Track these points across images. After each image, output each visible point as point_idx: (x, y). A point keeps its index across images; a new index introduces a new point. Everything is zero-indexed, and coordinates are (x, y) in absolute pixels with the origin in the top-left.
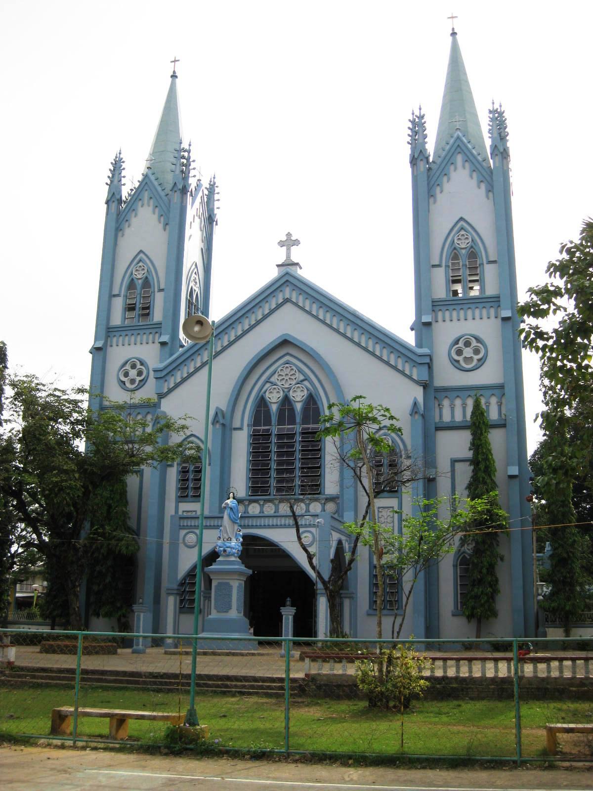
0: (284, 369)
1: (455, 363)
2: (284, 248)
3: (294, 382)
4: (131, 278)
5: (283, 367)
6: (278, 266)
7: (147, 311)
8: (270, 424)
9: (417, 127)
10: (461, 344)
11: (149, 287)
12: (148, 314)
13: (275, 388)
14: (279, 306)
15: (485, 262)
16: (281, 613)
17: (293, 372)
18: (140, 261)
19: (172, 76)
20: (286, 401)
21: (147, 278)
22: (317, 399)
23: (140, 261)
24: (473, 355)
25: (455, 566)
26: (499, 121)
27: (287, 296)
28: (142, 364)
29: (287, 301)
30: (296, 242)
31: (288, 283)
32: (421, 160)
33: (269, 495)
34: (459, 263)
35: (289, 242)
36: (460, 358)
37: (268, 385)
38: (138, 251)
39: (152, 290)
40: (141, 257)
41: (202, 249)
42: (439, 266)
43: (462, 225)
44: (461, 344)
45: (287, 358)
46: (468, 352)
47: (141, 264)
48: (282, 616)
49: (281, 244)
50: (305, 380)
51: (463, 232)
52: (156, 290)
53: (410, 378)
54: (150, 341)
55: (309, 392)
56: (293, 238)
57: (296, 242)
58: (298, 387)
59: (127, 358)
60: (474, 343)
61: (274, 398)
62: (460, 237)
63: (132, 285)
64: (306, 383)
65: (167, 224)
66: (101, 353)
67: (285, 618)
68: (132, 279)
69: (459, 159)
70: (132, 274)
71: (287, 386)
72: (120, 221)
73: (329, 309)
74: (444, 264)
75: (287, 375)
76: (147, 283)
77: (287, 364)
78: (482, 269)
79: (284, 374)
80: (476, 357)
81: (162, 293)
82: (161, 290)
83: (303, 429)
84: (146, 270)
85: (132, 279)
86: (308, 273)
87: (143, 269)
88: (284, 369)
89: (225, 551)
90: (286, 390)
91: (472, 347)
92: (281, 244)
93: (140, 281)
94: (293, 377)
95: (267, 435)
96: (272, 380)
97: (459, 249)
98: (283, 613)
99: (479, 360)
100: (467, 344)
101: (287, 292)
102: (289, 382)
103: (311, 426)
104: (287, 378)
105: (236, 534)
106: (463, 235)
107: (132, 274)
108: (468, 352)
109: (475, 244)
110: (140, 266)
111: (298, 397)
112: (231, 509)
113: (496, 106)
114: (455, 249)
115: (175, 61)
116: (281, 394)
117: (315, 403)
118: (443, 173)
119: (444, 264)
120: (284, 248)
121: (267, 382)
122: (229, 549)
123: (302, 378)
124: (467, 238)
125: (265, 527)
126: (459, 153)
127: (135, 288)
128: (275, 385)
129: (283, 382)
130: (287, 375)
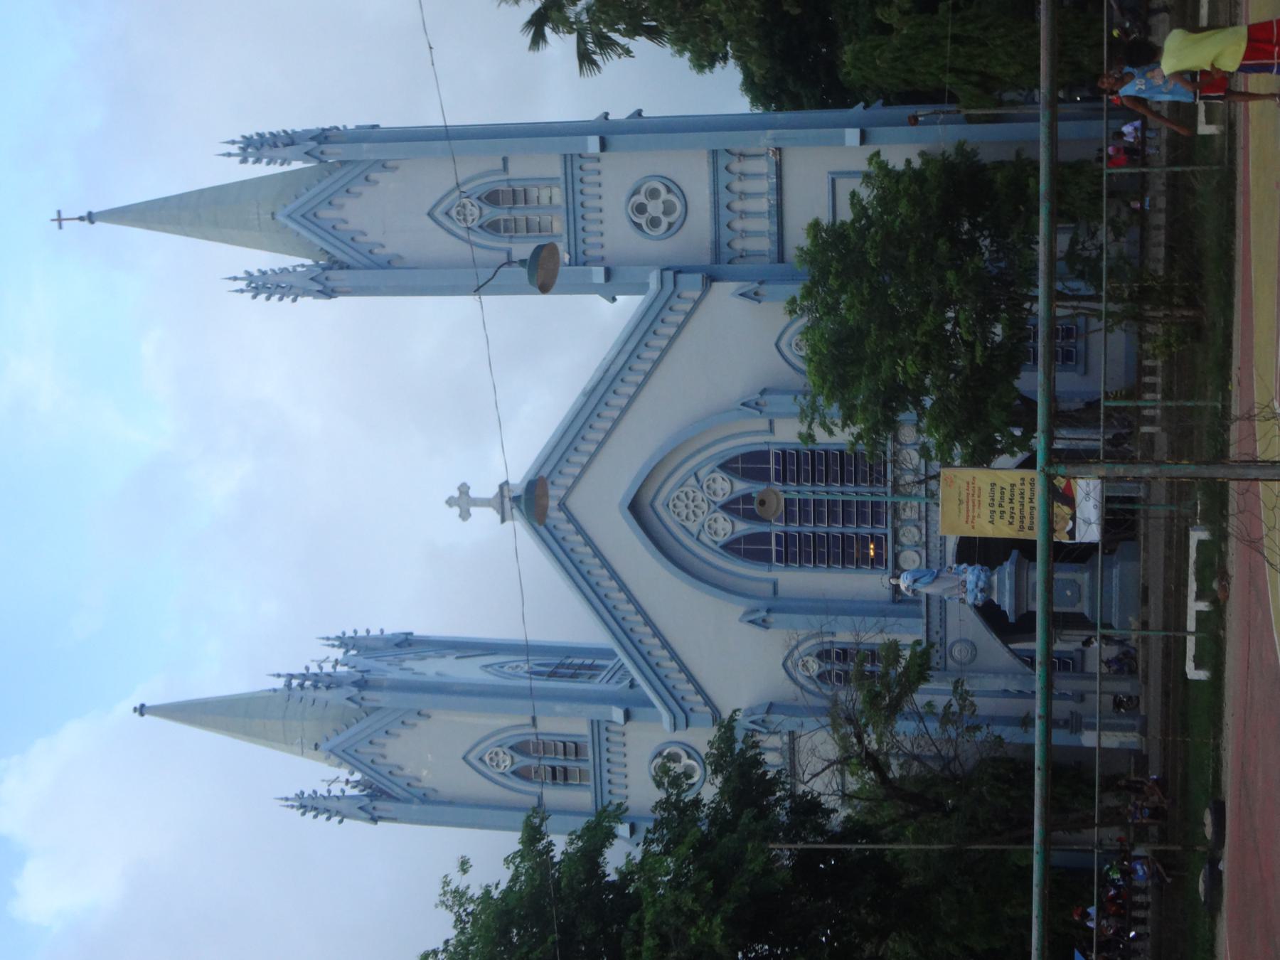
1: (672, 186)
2: (473, 510)
3: (699, 495)
4: (479, 230)
5: (674, 512)
8: (768, 535)
10: (642, 220)
13: (709, 527)
14: (571, 519)
17: (683, 496)
21: (511, 748)
23: (481, 759)
24: (660, 201)
26: (255, 147)
28: (638, 226)
29: (563, 506)
30: (464, 489)
33: (886, 535)
36: (665, 221)
38: (463, 763)
41: (457, 658)
43: (474, 761)
44: (642, 220)
46: (655, 208)
47: (487, 759)
49: (465, 515)
50: (696, 475)
51: (453, 213)
53: (697, 303)
55: (718, 470)
56: (456, 494)
57: (464, 489)
61: (726, 527)
64: (701, 474)
68: (514, 773)
69: (326, 214)
71: (705, 506)
73: (580, 436)
75: (687, 506)
76: (519, 748)
77: (668, 505)
80: (664, 195)
83: (777, 479)
84: (498, 749)
85: (481, 227)
86: (518, 476)
92: (465, 515)
93: (518, 758)
94: (691, 495)
99: (669, 190)
102: (699, 502)
103: (772, 466)
104: (692, 505)
107: (502, 774)
108: (655, 208)
110: (491, 759)
111: (726, 487)
113: (235, 149)
115: (59, 220)
116: (720, 515)
117: (735, 460)
119: (505, 245)
120: (473, 510)
123: (692, 481)
127: (528, 768)
128: (703, 526)
129: (699, 512)
130: (687, 506)
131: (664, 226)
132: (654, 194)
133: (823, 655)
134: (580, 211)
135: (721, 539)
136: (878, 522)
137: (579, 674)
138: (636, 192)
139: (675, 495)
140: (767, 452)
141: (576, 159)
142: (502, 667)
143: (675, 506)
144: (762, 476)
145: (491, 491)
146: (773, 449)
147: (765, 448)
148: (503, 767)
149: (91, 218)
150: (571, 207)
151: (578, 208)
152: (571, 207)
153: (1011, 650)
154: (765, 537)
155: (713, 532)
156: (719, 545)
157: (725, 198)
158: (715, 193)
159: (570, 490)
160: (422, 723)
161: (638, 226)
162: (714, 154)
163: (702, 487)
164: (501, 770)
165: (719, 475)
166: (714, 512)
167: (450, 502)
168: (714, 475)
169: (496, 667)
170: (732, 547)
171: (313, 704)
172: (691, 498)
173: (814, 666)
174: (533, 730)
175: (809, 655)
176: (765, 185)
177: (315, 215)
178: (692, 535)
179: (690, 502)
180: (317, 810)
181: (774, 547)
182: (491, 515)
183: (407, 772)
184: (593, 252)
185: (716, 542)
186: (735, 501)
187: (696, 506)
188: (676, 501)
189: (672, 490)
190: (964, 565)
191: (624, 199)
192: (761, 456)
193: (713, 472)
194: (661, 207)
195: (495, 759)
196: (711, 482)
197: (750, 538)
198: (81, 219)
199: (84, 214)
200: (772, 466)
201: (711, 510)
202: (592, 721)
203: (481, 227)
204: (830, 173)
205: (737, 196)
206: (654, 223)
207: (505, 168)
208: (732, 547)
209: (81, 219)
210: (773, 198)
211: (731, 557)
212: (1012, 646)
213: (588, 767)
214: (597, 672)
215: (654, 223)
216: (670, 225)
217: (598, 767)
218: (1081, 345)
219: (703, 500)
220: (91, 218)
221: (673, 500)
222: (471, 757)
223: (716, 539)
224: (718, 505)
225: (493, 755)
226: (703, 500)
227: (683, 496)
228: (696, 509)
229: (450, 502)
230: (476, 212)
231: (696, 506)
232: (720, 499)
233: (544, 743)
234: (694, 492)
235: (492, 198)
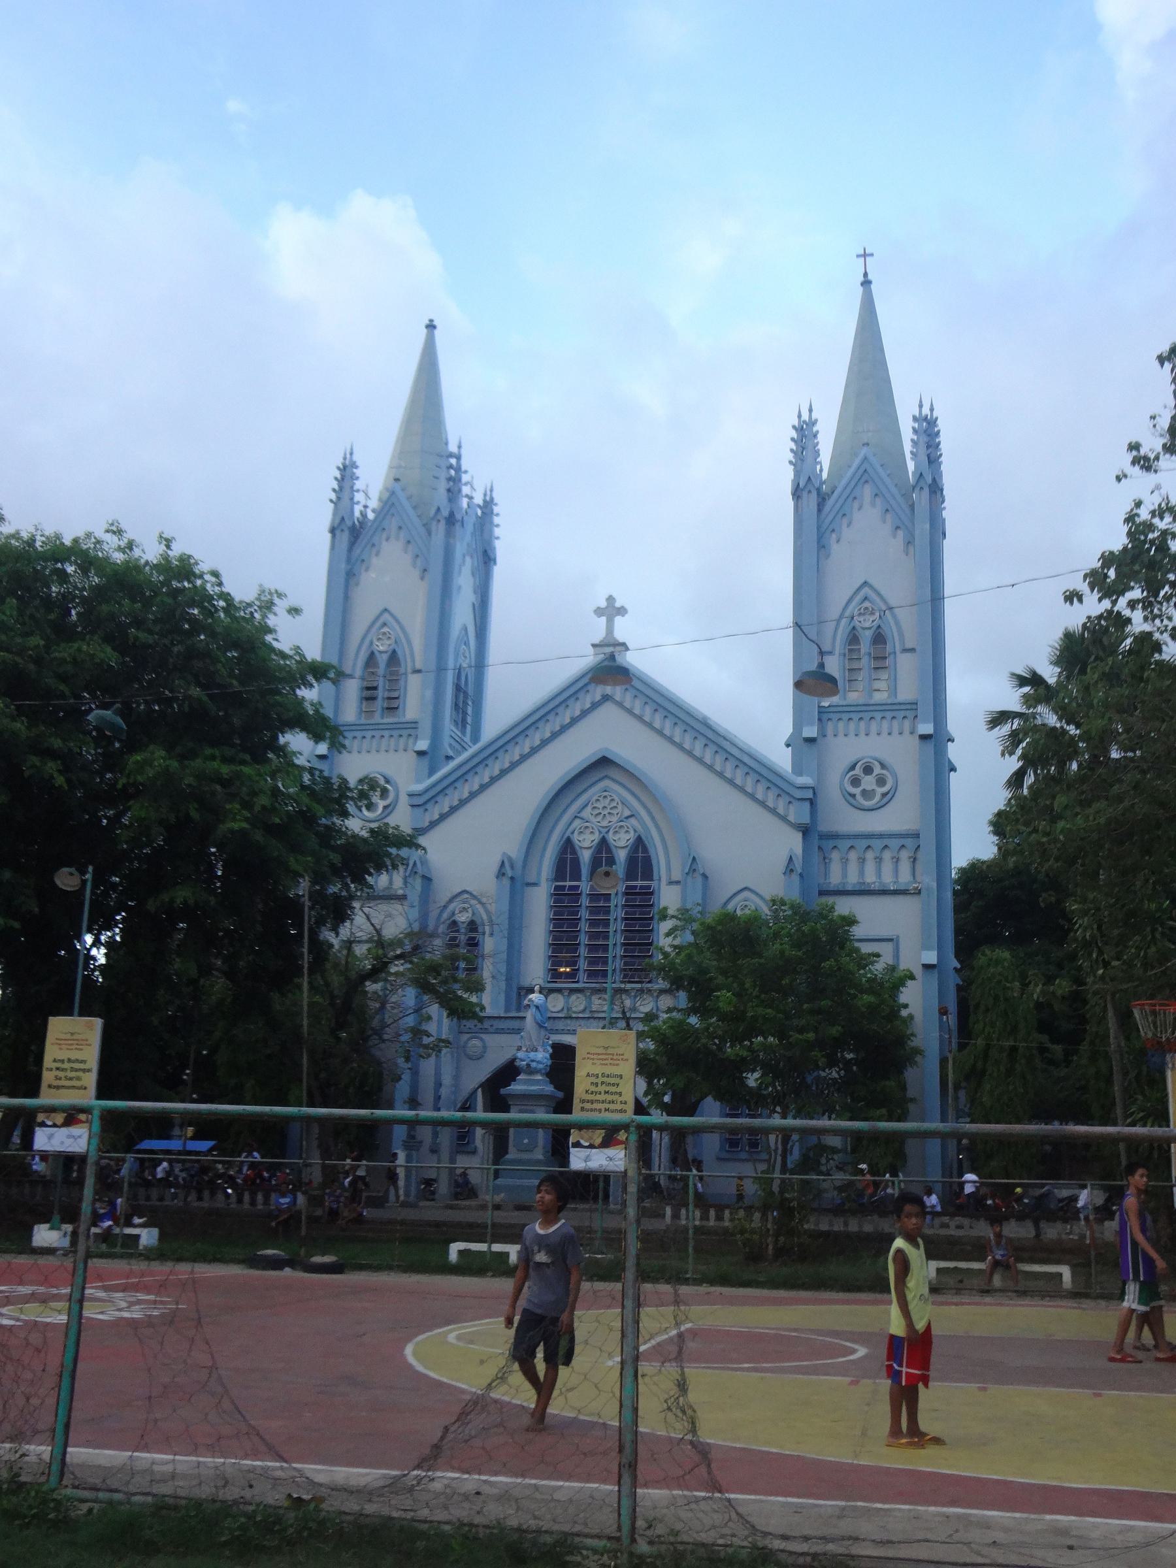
3: (615, 819)
6: (594, 646)
8: (579, 879)
9: (805, 434)
10: (858, 771)
14: (595, 706)
18: (866, 598)
19: (428, 327)
20: (603, 848)
23: (385, 624)
24: (874, 787)
26: (928, 429)
29: (606, 698)
30: (622, 611)
35: (612, 610)
36: (857, 791)
38: (381, 608)
41: (474, 604)
44: (858, 771)
46: (868, 782)
47: (385, 629)
49: (599, 612)
53: (784, 818)
54: (852, 733)
56: (618, 605)
57: (622, 611)
59: (853, 759)
61: (586, 843)
63: (371, 660)
64: (633, 821)
69: (867, 491)
71: (605, 823)
74: (837, 652)
76: (394, 659)
80: (880, 790)
85: (854, 628)
86: (633, 659)
88: (601, 799)
91: (874, 774)
92: (599, 612)
93: (385, 657)
94: (614, 812)
95: (575, 894)
96: (582, 815)
97: (859, 629)
99: (884, 795)
103: (639, 883)
108: (868, 782)
111: (621, 842)
112: (537, 1007)
113: (926, 411)
116: (596, 837)
117: (645, 850)
118: (863, 480)
119: (837, 652)
121: (576, 817)
123: (627, 813)
127: (376, 665)
129: (599, 818)
132: (881, 781)
133: (473, 926)
134: (867, 716)
135: (576, 838)
136: (589, 976)
138: (883, 766)
139: (615, 797)
142: (465, 644)
143: (605, 797)
144: (631, 874)
145: (620, 635)
146: (654, 884)
147: (655, 876)
149: (866, 283)
151: (902, 714)
153: (475, 1091)
154: (576, 876)
157: (877, 844)
158: (881, 836)
159: (620, 705)
161: (853, 767)
162: (916, 836)
165: (632, 836)
166: (600, 832)
167: (611, 599)
170: (568, 847)
173: (463, 918)
174: (409, 670)
175: (474, 914)
176: (888, 880)
177: (866, 482)
180: (341, 481)
181: (568, 884)
182: (599, 635)
184: (830, 727)
185: (573, 833)
188: (609, 798)
189: (619, 795)
190: (551, 1050)
191: (878, 755)
192: (648, 873)
193: (635, 831)
194: (869, 788)
197: (576, 862)
198: (866, 274)
199: (870, 277)
200: (639, 883)
201: (601, 829)
202: (416, 722)
203: (854, 628)
204: (898, 937)
206: (856, 782)
207: (905, 650)
209: (866, 274)
210: (877, 887)
212: (480, 1090)
213: (377, 718)
215: (856, 782)
216: (853, 796)
217: (377, 727)
220: (866, 283)
224: (606, 836)
229: (611, 599)
230: (867, 625)
232: (611, 837)
235: (879, 638)
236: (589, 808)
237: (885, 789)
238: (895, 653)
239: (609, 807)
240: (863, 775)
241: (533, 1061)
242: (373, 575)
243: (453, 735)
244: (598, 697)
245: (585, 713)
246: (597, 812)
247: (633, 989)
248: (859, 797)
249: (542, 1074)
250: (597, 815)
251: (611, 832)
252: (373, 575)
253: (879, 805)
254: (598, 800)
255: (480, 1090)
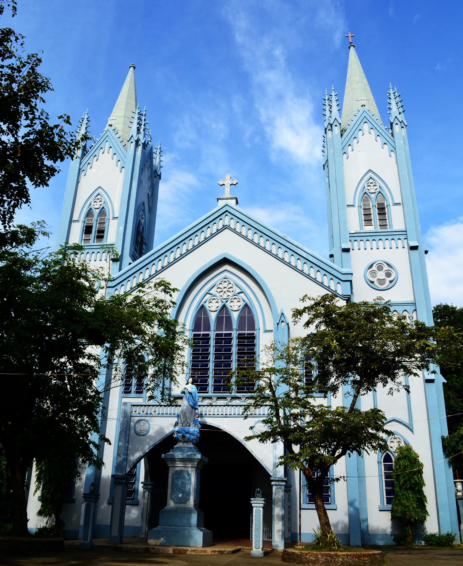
0: (222, 283)
3: (231, 294)
5: (222, 281)
7: (101, 235)
8: (209, 330)
10: (374, 268)
11: (105, 215)
12: (102, 237)
13: (214, 299)
14: (219, 231)
15: (391, 204)
16: (251, 504)
17: (230, 286)
22: (252, 310)
24: (385, 277)
25: (379, 463)
27: (227, 223)
29: (225, 227)
31: (227, 213)
32: (336, 126)
33: (207, 393)
34: (369, 205)
36: (375, 280)
37: (208, 296)
38: (98, 186)
39: (107, 217)
40: (99, 192)
41: (148, 194)
42: (353, 206)
45: (226, 274)
47: (99, 197)
48: (252, 508)
50: (242, 292)
52: (111, 218)
55: (245, 303)
58: (235, 298)
60: (386, 268)
62: (369, 184)
63: (89, 214)
64: (242, 295)
65: (123, 167)
66: (118, 263)
67: (256, 512)
68: (91, 209)
69: (366, 127)
70: (91, 204)
71: (225, 296)
72: (83, 164)
74: (357, 205)
75: (225, 288)
76: (102, 212)
77: (225, 278)
78: (389, 209)
79: (222, 287)
81: (116, 221)
82: (114, 218)
83: (239, 334)
84: (103, 202)
85: (91, 209)
87: (101, 201)
88: (222, 283)
89: (183, 436)
90: (224, 301)
91: (384, 270)
93: (98, 211)
94: (231, 290)
95: (206, 338)
96: (211, 292)
97: (369, 194)
98: (253, 505)
99: (391, 282)
100: (380, 268)
101: (226, 220)
103: (246, 332)
104: (225, 290)
105: (194, 420)
106: (371, 183)
107: (91, 204)
109: (381, 189)
110: (98, 199)
112: (190, 393)
114: (365, 193)
116: (220, 305)
117: (250, 312)
118: (358, 129)
119: (357, 205)
121: (207, 293)
122: (188, 435)
123: (239, 291)
124: (375, 185)
125: (218, 416)
126: (365, 122)
127: (93, 216)
128: (214, 296)
129: (221, 294)
130: (225, 288)
131: (372, 279)
132: (388, 275)
134: (377, 238)
135: (207, 305)
137: (138, 245)
140: (254, 329)
141: (405, 236)
142: (143, 210)
143: (225, 282)
144: (241, 326)
146: (255, 332)
147: (256, 327)
148: (94, 204)
150: (379, 234)
152: (379, 234)
153: (139, 460)
154: (208, 328)
155: (232, 300)
156: (204, 304)
159: (234, 231)
160: (119, 168)
163: (235, 295)
164: (92, 203)
165: (242, 304)
166: (222, 302)
168: (242, 301)
169: (143, 208)
170: (202, 309)
171: (131, 122)
172: (229, 290)
174: (111, 218)
178: (209, 291)
179: (227, 289)
181: (202, 333)
183: (95, 163)
185: (205, 302)
186: (227, 312)
187: (225, 292)
188: (228, 282)
192: (252, 325)
193: (244, 301)
194: (381, 278)
195: (98, 201)
196: (217, 301)
201: (222, 300)
205: (411, 315)
207: (396, 204)
208: (202, 309)
211: (233, 318)
212: (143, 461)
213: (91, 243)
214: (138, 253)
215: (373, 273)
216: (372, 282)
218: (96, 234)
219: (228, 296)
221: (228, 281)
222: (100, 191)
223: (207, 302)
224: (226, 304)
225: (100, 200)
226: (228, 296)
227: (230, 286)
228: (223, 292)
231: (225, 292)
232: (228, 304)
233: (105, 223)
234: (233, 291)
236: (215, 288)
237: (391, 279)
238: (109, 219)
239: (227, 288)
240: (377, 271)
241: (187, 433)
242: (94, 171)
243: (134, 255)
244: (221, 227)
245: (213, 236)
246: (220, 290)
247: (244, 396)
248: (376, 283)
249: (193, 444)
250: (220, 292)
251: (229, 302)
252: (94, 171)
253: (386, 288)
254: (220, 284)
255: (143, 461)
